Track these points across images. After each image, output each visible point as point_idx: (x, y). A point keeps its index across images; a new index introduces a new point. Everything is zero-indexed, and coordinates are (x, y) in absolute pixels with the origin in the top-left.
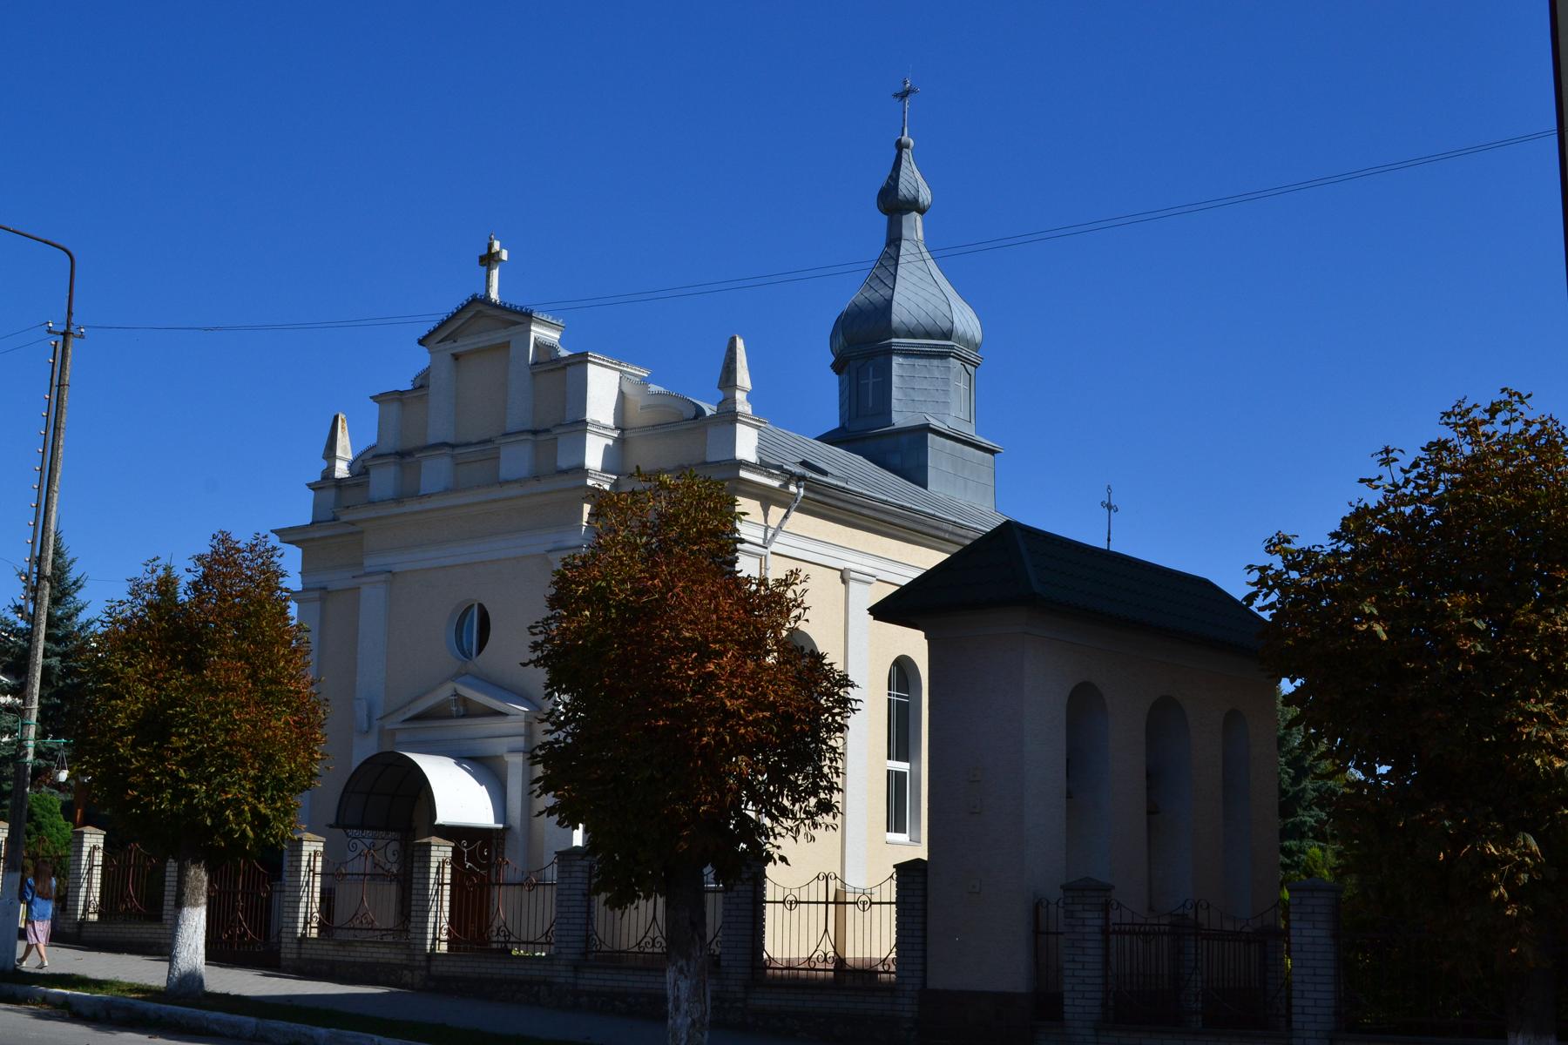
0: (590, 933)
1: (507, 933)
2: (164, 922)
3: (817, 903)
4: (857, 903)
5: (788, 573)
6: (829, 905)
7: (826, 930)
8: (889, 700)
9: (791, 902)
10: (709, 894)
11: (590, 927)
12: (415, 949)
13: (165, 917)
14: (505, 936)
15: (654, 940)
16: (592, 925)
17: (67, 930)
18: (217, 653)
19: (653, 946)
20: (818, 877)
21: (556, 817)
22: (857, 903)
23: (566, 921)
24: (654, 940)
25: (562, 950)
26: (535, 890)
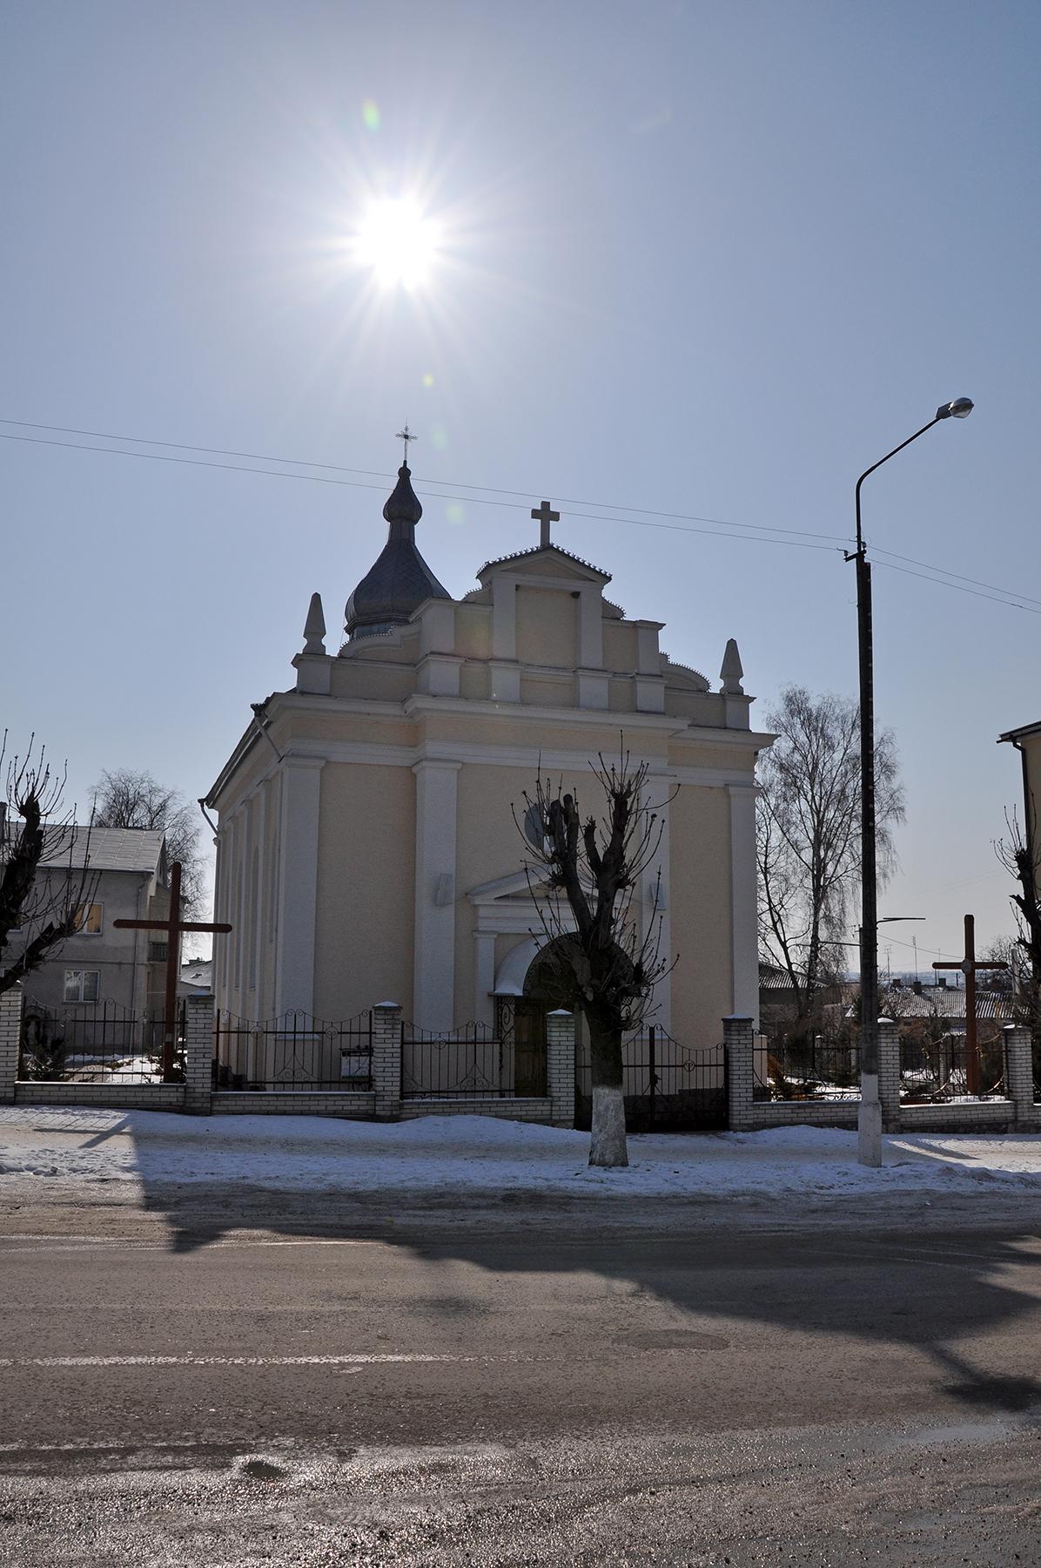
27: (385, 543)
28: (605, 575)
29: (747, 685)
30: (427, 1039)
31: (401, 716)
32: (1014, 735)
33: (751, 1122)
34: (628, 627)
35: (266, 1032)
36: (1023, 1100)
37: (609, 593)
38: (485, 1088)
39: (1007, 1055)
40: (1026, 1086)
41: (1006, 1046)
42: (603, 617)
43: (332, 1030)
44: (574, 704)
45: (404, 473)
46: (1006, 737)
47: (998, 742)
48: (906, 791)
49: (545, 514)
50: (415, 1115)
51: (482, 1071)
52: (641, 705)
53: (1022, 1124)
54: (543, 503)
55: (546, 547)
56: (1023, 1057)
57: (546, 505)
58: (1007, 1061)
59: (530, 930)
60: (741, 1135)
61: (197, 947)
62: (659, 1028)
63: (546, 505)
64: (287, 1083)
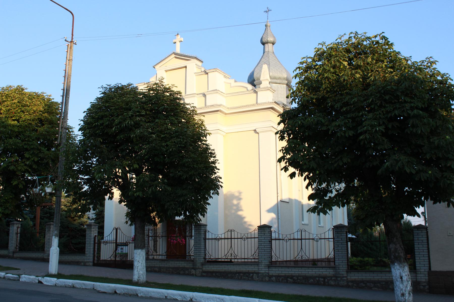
0: (149, 249)
1: (235, 256)
2: (86, 254)
3: (234, 238)
5: (206, 127)
7: (231, 246)
9: (286, 240)
11: (149, 247)
12: (196, 262)
13: (86, 252)
14: (234, 256)
16: (149, 246)
17: (45, 257)
19: (231, 256)
20: (298, 231)
21: (95, 215)
23: (263, 251)
25: (262, 261)
30: (213, 237)
36: (262, 262)
38: (235, 257)
40: (264, 255)
43: (244, 237)
48: (38, 92)
51: (208, 251)
53: (261, 274)
56: (262, 240)
61: (427, 219)
62: (119, 228)
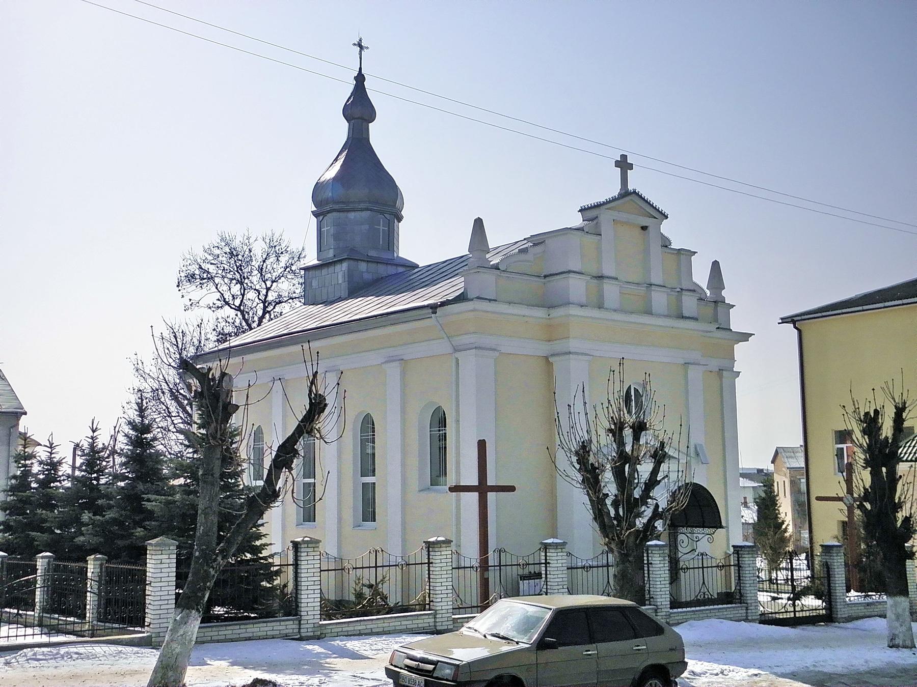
4: (398, 565)
6: (374, 565)
8: (445, 427)
9: (523, 565)
10: (292, 563)
15: (704, 594)
18: (767, 542)
22: (398, 565)
24: (704, 594)
26: (591, 571)
27: (345, 140)
28: (664, 215)
29: (728, 295)
31: (546, 318)
32: (795, 319)
33: (846, 616)
34: (674, 253)
35: (356, 568)
37: (665, 228)
39: (648, 567)
41: (648, 560)
42: (662, 246)
44: (649, 312)
45: (360, 79)
46: (784, 320)
47: (779, 323)
49: (624, 165)
50: (685, 620)
52: (686, 314)
54: (622, 156)
55: (626, 193)
57: (624, 157)
58: (546, 572)
59: (837, 494)
60: (842, 624)
63: (624, 157)
64: (467, 608)
